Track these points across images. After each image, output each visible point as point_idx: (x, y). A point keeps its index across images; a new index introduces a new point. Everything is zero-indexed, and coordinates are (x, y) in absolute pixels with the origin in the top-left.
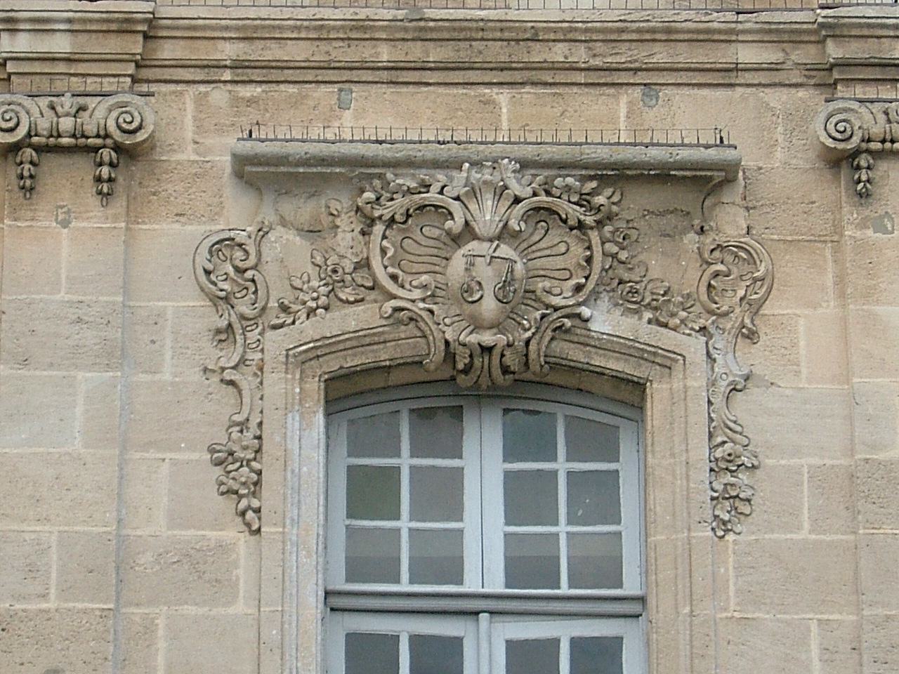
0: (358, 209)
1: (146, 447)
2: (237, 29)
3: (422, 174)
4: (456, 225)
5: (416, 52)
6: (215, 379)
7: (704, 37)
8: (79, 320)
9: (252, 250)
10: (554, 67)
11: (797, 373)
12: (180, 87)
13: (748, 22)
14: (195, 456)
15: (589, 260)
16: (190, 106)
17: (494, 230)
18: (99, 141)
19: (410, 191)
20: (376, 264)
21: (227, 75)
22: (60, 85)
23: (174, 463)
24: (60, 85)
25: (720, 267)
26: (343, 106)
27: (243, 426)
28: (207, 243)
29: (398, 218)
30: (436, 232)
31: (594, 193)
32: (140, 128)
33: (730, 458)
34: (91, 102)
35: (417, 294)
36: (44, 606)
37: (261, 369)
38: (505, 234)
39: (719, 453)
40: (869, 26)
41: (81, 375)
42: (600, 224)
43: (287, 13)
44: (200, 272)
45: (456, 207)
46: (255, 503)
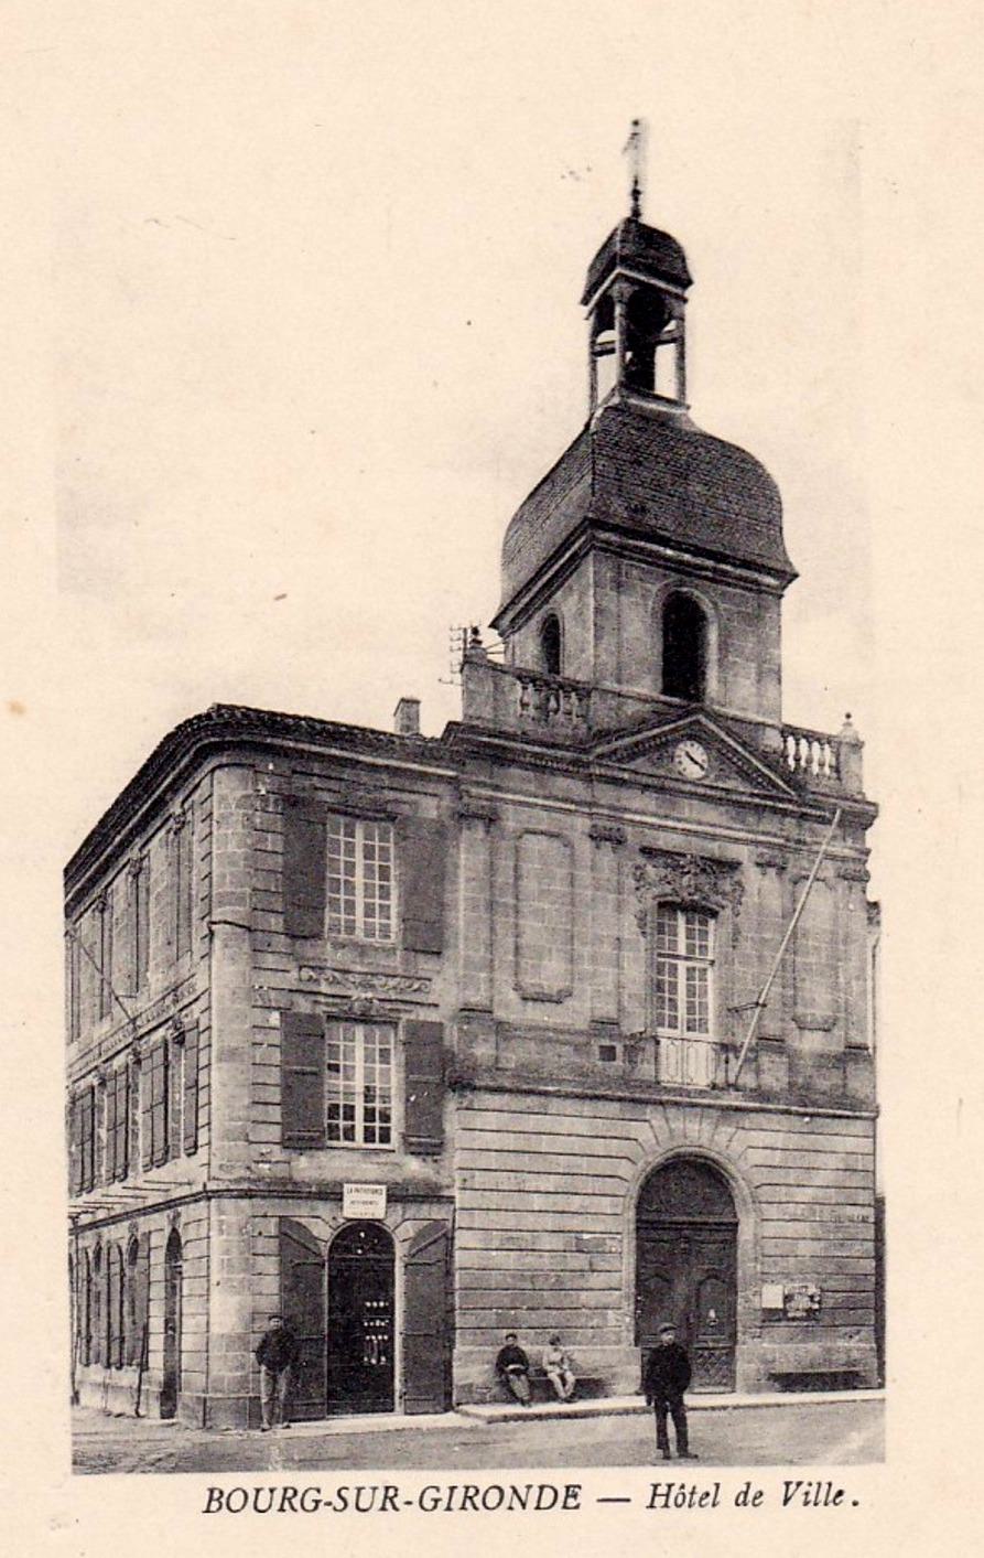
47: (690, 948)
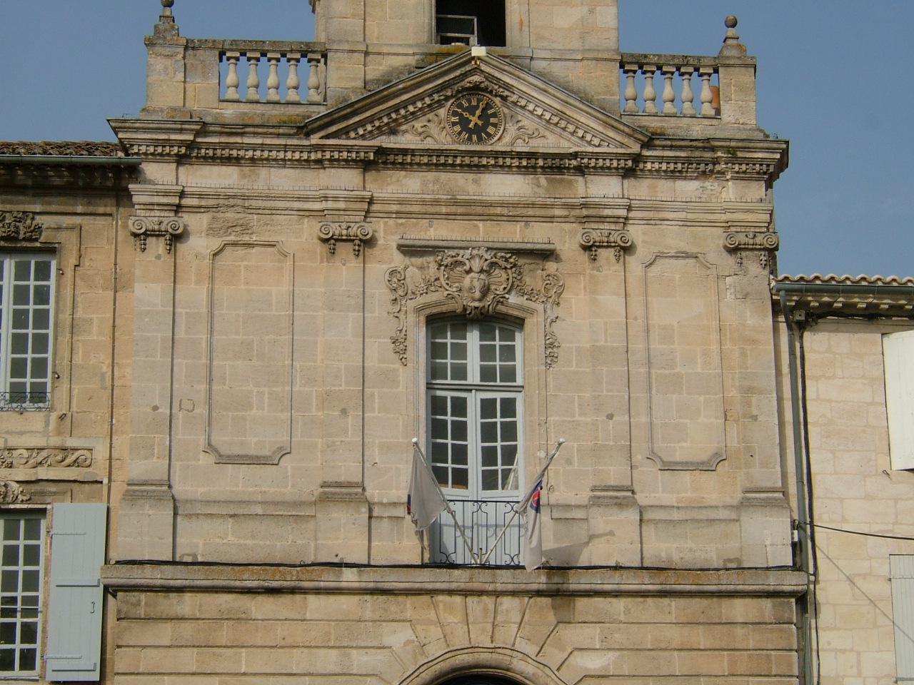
0: (436, 261)
1: (371, 337)
2: (397, 201)
3: (456, 251)
4: (467, 268)
5: (453, 209)
6: (392, 315)
7: (544, 206)
8: (349, 296)
9: (403, 273)
10: (497, 215)
11: (572, 316)
12: (379, 219)
13: (559, 202)
14: (386, 340)
15: (508, 279)
16: (382, 226)
17: (478, 270)
18: (354, 238)
19: (453, 257)
20: (442, 279)
21: (394, 216)
22: (342, 219)
23: (379, 342)
24: (342, 219)
25: (549, 282)
26: (431, 226)
27: (401, 331)
28: (389, 271)
29: (449, 265)
30: (461, 269)
31: (510, 257)
32: (368, 234)
33: (551, 344)
34: (352, 225)
35: (455, 290)
36: (341, 388)
37: (406, 313)
38: (482, 271)
39: (548, 342)
40: (596, 205)
41: (350, 314)
42: (511, 268)
43: (413, 196)
44: (386, 281)
45: (467, 262)
46: (405, 356)
47: (487, 374)
